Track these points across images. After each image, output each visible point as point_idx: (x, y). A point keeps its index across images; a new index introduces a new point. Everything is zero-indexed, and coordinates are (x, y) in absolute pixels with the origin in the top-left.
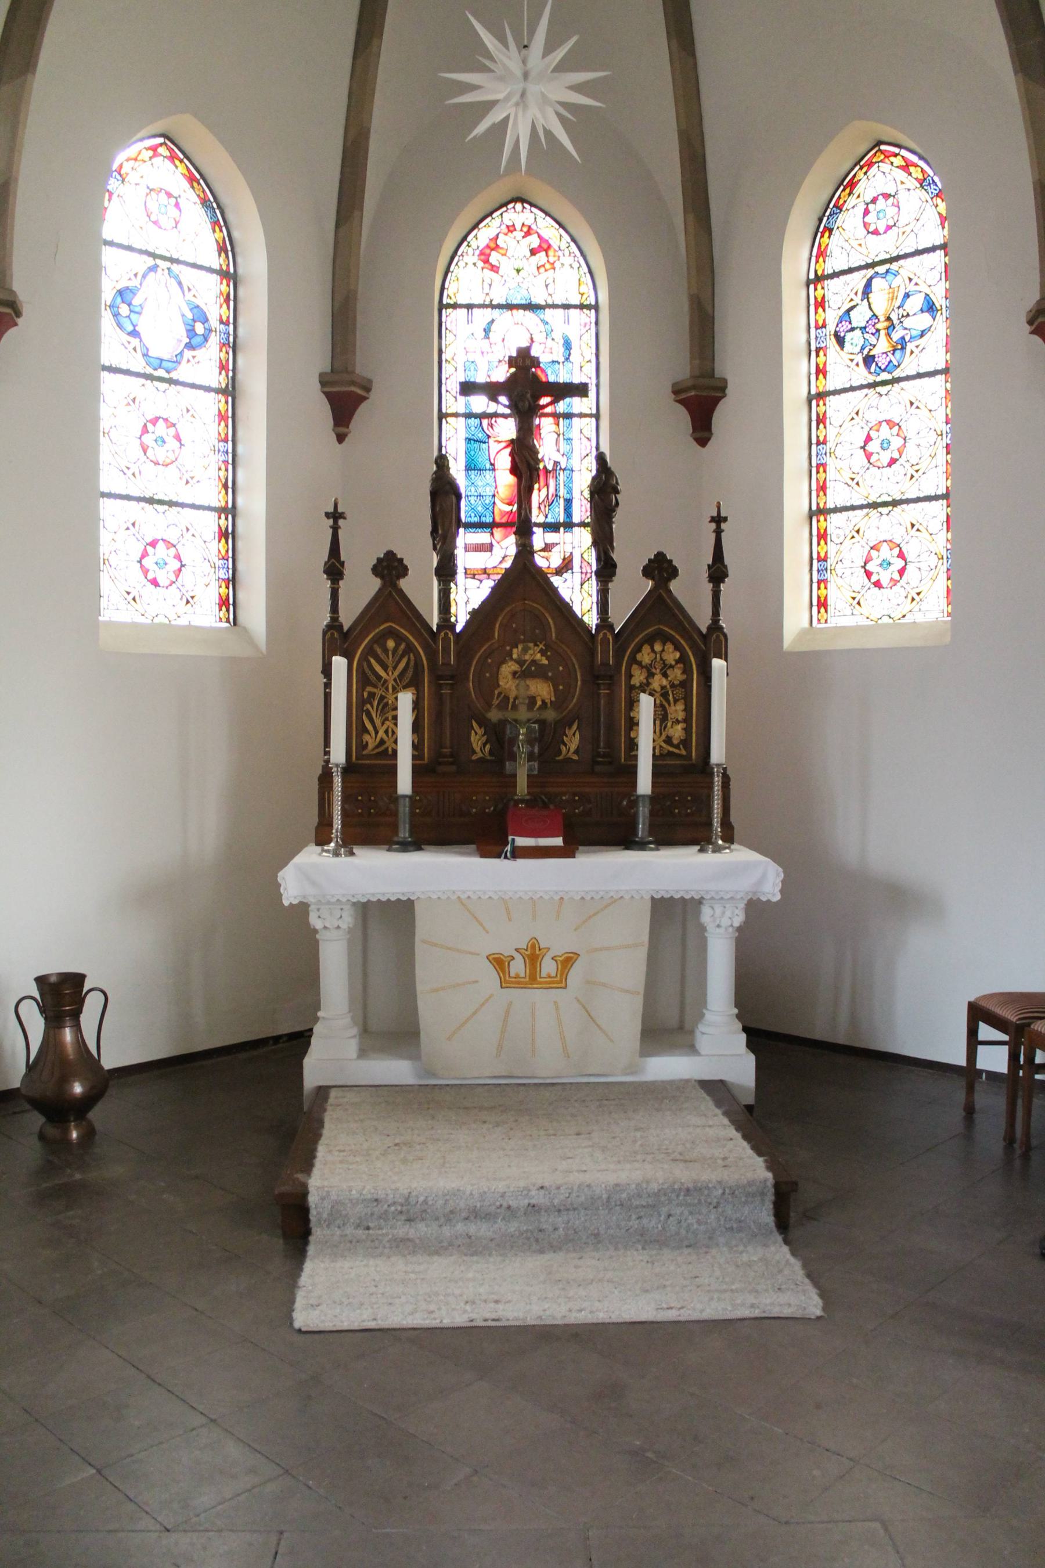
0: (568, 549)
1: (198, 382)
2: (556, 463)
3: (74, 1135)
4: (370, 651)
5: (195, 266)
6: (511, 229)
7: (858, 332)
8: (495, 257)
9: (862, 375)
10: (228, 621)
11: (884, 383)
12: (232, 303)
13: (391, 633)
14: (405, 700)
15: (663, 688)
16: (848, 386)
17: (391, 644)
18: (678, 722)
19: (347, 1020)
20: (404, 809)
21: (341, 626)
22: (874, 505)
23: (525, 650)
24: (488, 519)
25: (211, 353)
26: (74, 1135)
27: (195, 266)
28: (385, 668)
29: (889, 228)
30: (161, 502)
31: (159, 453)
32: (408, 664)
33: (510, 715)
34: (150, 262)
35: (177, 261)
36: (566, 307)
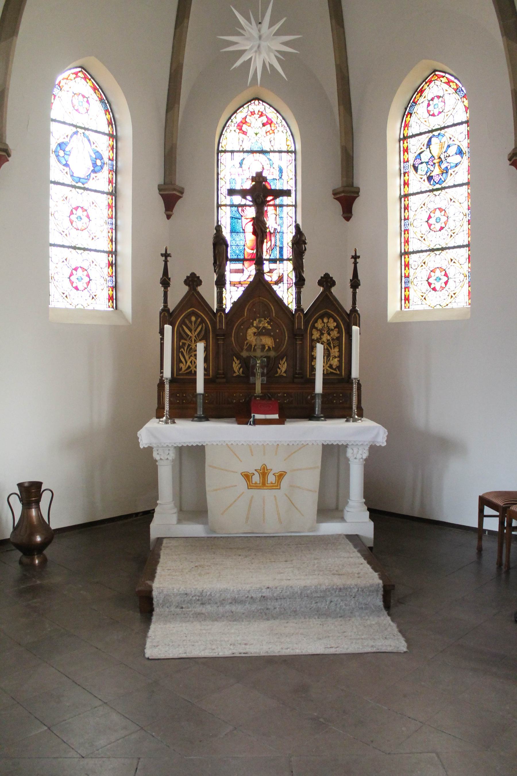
0: (281, 272)
1: (98, 189)
2: (275, 229)
3: (37, 562)
4: (183, 322)
5: (96, 132)
6: (253, 113)
7: (424, 164)
8: (245, 127)
9: (427, 186)
10: (113, 307)
11: (437, 190)
12: (115, 150)
13: (193, 313)
14: (200, 347)
15: (328, 340)
16: (419, 191)
17: (193, 319)
18: (335, 357)
19: (172, 505)
20: (200, 401)
21: (169, 310)
22: (433, 250)
23: (260, 322)
24: (242, 257)
25: (105, 175)
26: (37, 562)
27: (96, 132)
28: (190, 330)
29: (440, 113)
30: (79, 249)
31: (79, 224)
32: (202, 329)
33: (252, 354)
34: (74, 129)
35: (88, 129)
36: (280, 152)
